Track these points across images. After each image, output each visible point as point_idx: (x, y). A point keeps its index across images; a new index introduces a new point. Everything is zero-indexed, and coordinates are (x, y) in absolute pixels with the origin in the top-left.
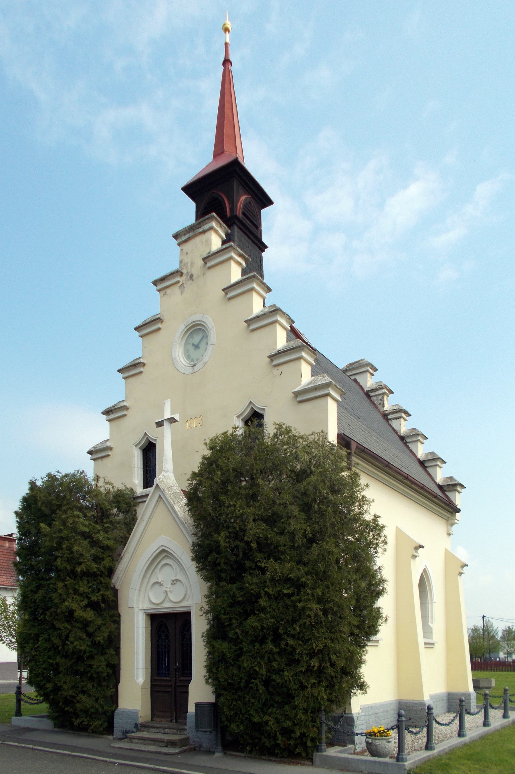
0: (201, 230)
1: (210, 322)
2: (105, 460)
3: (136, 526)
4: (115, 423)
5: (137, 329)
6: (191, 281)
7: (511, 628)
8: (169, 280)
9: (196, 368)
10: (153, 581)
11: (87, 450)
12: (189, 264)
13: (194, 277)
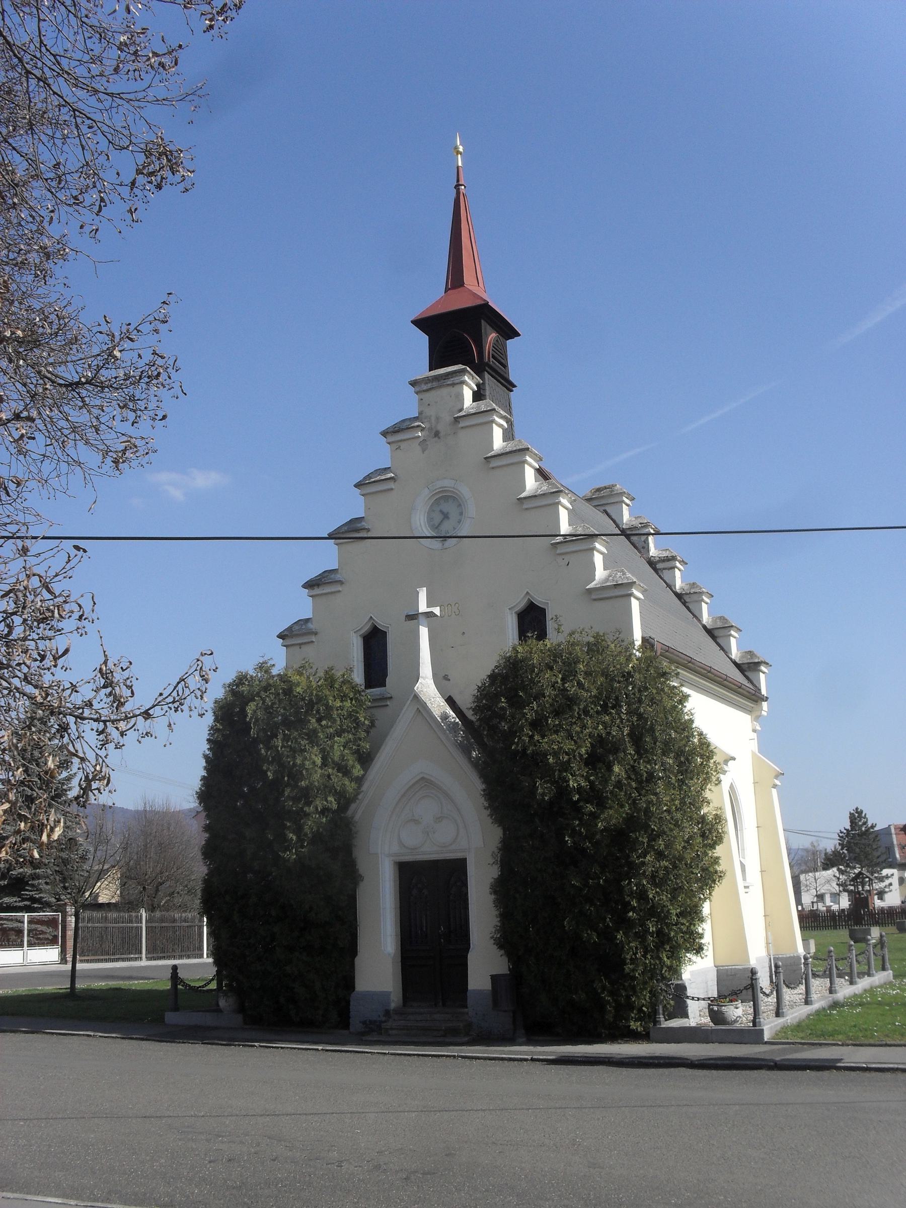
1: (465, 491)
7: (816, 844)
13: (441, 435)
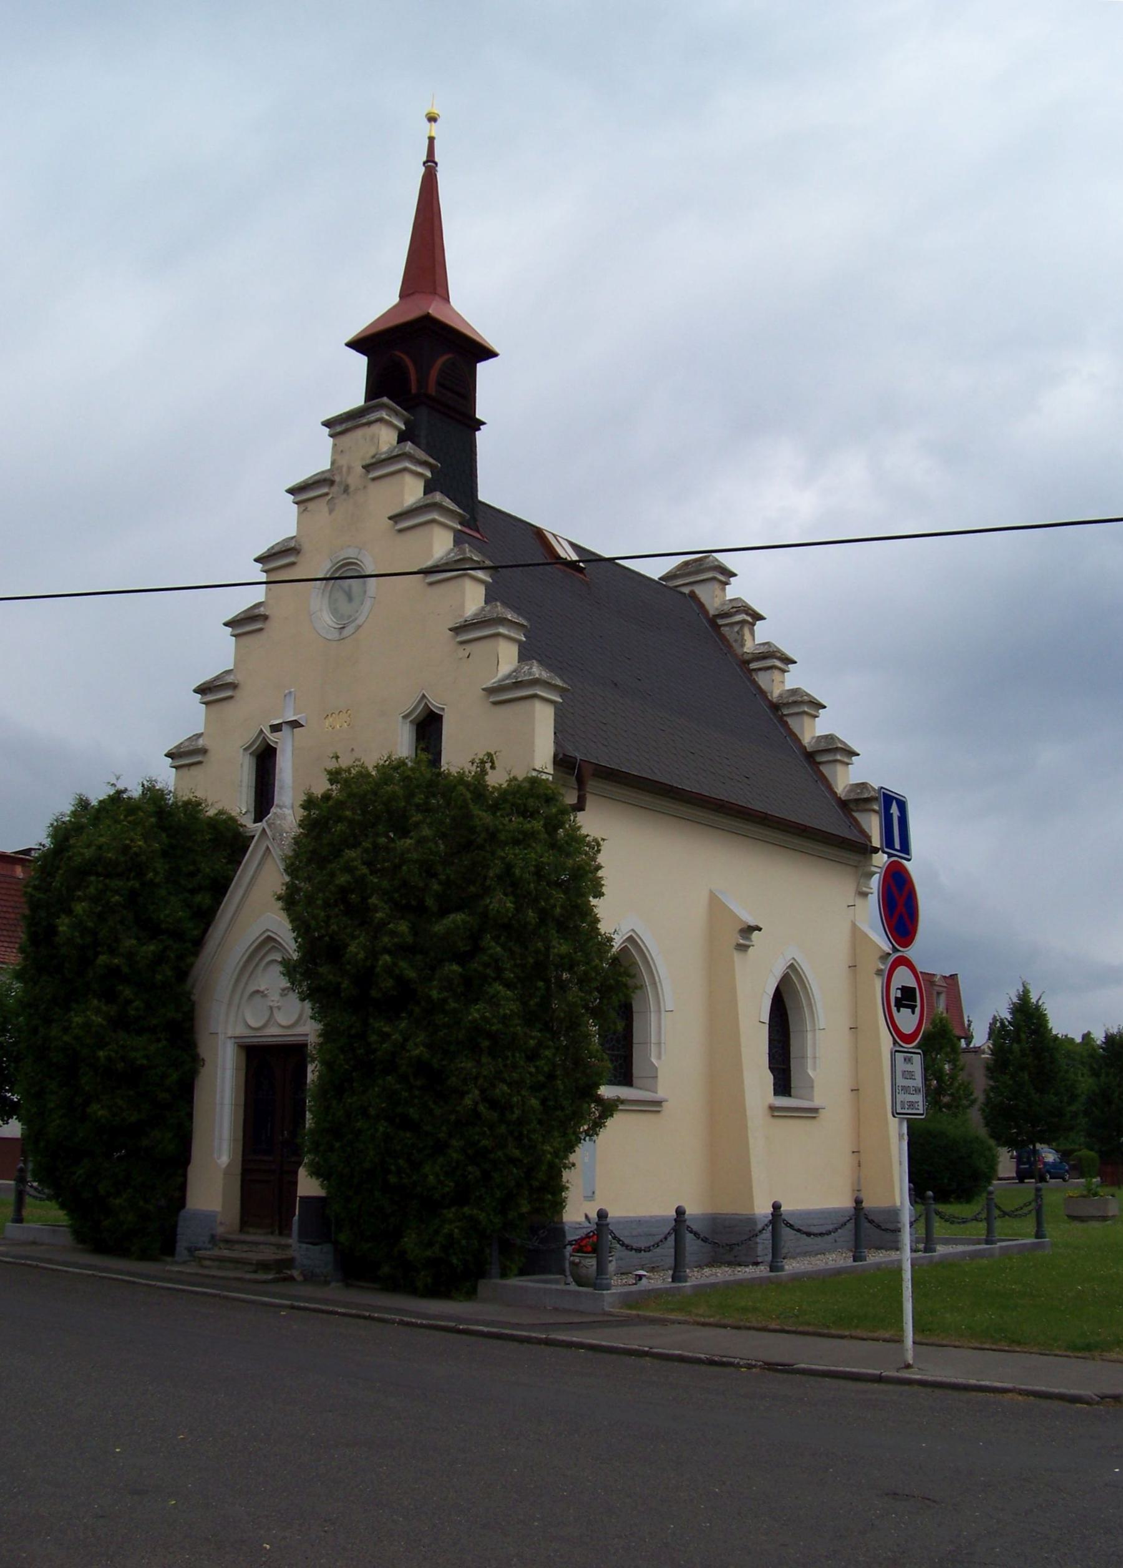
0: (364, 420)
2: (194, 771)
3: (231, 889)
4: (215, 708)
5: (291, 491)
6: (345, 496)
8: (312, 489)
9: (346, 632)
10: (252, 988)
11: (194, 687)
12: (344, 469)
13: (352, 489)
